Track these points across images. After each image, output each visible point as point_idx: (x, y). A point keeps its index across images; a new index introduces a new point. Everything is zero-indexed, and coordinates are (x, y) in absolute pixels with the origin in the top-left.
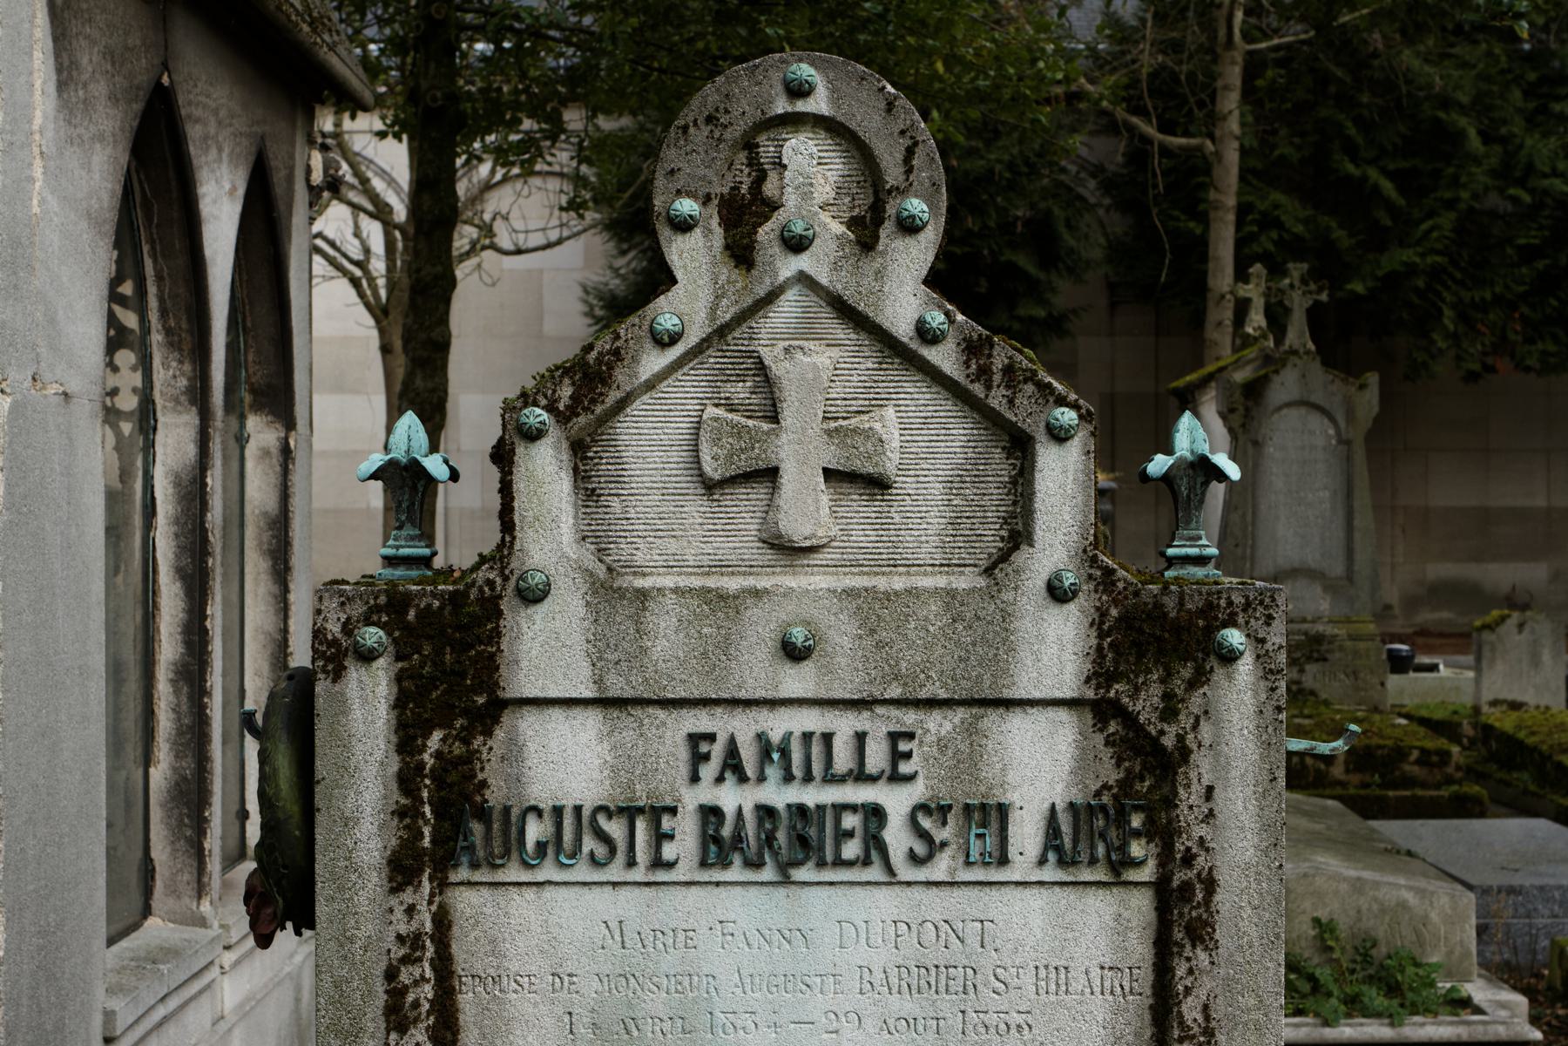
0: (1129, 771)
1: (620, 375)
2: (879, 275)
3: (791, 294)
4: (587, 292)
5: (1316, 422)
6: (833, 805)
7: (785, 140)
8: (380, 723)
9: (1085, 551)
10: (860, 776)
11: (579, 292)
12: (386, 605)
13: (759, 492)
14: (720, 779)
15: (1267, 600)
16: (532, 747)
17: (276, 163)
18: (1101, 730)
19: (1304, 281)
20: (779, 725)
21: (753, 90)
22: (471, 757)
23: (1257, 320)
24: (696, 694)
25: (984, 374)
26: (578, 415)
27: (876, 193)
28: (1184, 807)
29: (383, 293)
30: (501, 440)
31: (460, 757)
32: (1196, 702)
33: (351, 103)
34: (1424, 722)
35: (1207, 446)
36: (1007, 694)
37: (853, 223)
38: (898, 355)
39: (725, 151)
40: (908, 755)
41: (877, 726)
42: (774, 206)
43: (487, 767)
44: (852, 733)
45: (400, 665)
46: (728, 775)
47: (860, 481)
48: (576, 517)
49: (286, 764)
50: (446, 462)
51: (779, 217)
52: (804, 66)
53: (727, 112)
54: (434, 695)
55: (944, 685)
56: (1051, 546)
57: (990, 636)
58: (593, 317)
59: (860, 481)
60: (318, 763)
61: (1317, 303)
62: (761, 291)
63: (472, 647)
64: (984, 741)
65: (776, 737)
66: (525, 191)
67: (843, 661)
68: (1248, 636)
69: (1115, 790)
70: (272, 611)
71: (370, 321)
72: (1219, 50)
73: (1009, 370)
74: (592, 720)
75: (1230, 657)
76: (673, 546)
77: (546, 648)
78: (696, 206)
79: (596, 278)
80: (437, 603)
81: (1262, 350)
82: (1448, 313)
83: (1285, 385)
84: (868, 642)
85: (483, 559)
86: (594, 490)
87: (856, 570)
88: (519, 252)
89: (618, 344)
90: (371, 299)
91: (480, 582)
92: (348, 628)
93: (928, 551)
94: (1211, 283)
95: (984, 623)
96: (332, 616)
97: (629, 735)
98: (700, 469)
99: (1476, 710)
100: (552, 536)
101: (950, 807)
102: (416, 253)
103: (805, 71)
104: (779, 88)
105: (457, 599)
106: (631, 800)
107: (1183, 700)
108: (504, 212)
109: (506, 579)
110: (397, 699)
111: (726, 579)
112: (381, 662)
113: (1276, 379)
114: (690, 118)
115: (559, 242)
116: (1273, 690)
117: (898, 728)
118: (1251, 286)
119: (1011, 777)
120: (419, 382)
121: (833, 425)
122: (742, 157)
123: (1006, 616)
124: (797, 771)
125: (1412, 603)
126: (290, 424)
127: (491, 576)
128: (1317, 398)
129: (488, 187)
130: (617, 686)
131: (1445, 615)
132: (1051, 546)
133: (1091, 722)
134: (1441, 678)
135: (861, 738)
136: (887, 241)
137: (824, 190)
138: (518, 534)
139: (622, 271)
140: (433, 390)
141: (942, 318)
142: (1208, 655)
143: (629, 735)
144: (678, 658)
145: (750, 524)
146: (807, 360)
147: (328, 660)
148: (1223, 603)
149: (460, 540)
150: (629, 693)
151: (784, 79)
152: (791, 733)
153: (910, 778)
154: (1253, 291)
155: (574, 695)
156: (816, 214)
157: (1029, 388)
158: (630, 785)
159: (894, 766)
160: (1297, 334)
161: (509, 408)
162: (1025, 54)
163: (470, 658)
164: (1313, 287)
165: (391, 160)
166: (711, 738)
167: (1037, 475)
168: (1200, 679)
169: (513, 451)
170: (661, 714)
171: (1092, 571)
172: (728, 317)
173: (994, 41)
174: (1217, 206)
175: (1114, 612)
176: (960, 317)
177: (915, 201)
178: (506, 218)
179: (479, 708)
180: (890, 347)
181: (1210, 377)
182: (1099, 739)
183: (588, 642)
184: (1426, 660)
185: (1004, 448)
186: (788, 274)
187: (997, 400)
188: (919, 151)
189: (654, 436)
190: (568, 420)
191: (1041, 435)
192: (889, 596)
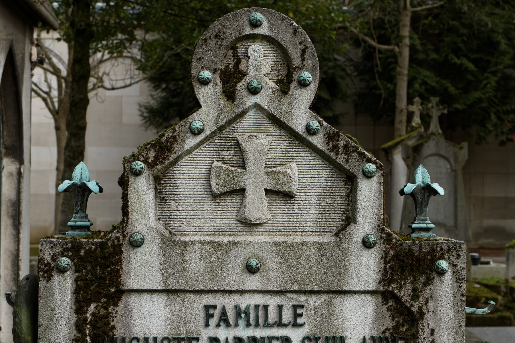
0: (397, 322)
1: (176, 147)
2: (290, 105)
3: (251, 113)
4: (140, 106)
5: (442, 162)
6: (268, 337)
7: (249, 46)
8: (68, 300)
9: (379, 226)
10: (280, 324)
11: (137, 107)
12: (71, 248)
13: (236, 199)
14: (218, 326)
15: (458, 248)
16: (135, 311)
17: (17, 51)
18: (385, 304)
19: (437, 105)
20: (245, 301)
21: (235, 24)
22: (108, 315)
23: (417, 120)
24: (208, 288)
25: (335, 148)
26: (157, 165)
27: (289, 69)
28: (421, 338)
29: (56, 105)
30: (123, 175)
31: (103, 315)
32: (427, 292)
33: (48, 26)
34: (486, 286)
35: (430, 180)
36: (345, 288)
37: (278, 82)
38: (298, 140)
39: (223, 50)
40: (301, 315)
41: (288, 302)
42: (244, 74)
43: (115, 320)
44: (276, 305)
45: (77, 274)
46: (222, 323)
47: (281, 195)
48: (156, 210)
49: (25, 318)
50: (97, 184)
51: (246, 79)
52: (258, 14)
53: (224, 33)
54: (92, 288)
55: (317, 285)
56: (364, 224)
57: (337, 263)
58: (143, 116)
59: (281, 195)
60: (40, 318)
61: (443, 114)
62: (238, 111)
63: (109, 266)
64: (334, 309)
65: (243, 307)
66: (116, 64)
67: (273, 274)
68: (449, 263)
69: (391, 331)
70: (12, 241)
71: (50, 115)
72: (401, 10)
73: (346, 147)
74: (161, 300)
75: (441, 273)
76: (198, 222)
77: (142, 268)
78: (210, 74)
79: (144, 101)
80: (94, 247)
81: (419, 132)
82: (493, 116)
83: (430, 148)
84: (284, 265)
85: (114, 228)
86: (164, 198)
87: (279, 233)
88: (113, 89)
89: (175, 134)
90: (51, 107)
91: (113, 238)
92: (54, 258)
93: (310, 226)
94: (397, 105)
95: (334, 257)
96: (47, 253)
97: (178, 306)
98: (211, 189)
99: (507, 281)
100: (145, 217)
101: (319, 338)
102: (73, 89)
103: (258, 16)
104: (247, 23)
105: (102, 246)
106: (179, 334)
107: (421, 292)
108: (107, 72)
109: (124, 237)
110: (76, 290)
111: (221, 237)
112: (68, 273)
113: (426, 145)
114: (208, 36)
115: (130, 85)
116: (460, 287)
117: (297, 303)
118: (414, 107)
119: (346, 325)
120: (73, 143)
121: (269, 170)
122: (230, 52)
123: (344, 254)
124: (252, 322)
125: (477, 236)
126: (21, 162)
127: (118, 235)
128: (443, 152)
129: (101, 61)
130: (173, 285)
131: (491, 240)
132: (364, 224)
133: (381, 301)
134: (491, 268)
135: (280, 308)
136: (294, 90)
137: (266, 68)
138: (130, 217)
139: (155, 97)
140: (79, 147)
141: (317, 124)
142: (432, 272)
143: (178, 306)
144: (200, 272)
145: (232, 213)
146: (258, 141)
147: (45, 272)
148: (438, 249)
149: (100, 214)
150: (178, 287)
151: (249, 19)
152: (250, 305)
153: (302, 325)
154: (416, 108)
155: (154, 288)
156: (263, 78)
157: (355, 155)
158: (179, 328)
159: (295, 319)
160: (434, 126)
161: (126, 161)
162: (326, 10)
163: (108, 272)
164: (441, 107)
165: (59, 49)
166: (214, 307)
167: (358, 193)
168: (429, 282)
169: (128, 180)
170: (192, 296)
171: (382, 235)
172: (224, 122)
173: (313, 5)
174: (400, 74)
175: (391, 253)
176: (325, 124)
177: (306, 73)
178: (108, 75)
179: (112, 294)
180: (295, 136)
181: (397, 144)
182: (385, 308)
183: (161, 264)
184: (483, 259)
185: (343, 181)
186: (250, 104)
187: (341, 160)
188: (308, 51)
189: (190, 175)
190: (153, 167)
191: (360, 175)
192: (293, 245)
